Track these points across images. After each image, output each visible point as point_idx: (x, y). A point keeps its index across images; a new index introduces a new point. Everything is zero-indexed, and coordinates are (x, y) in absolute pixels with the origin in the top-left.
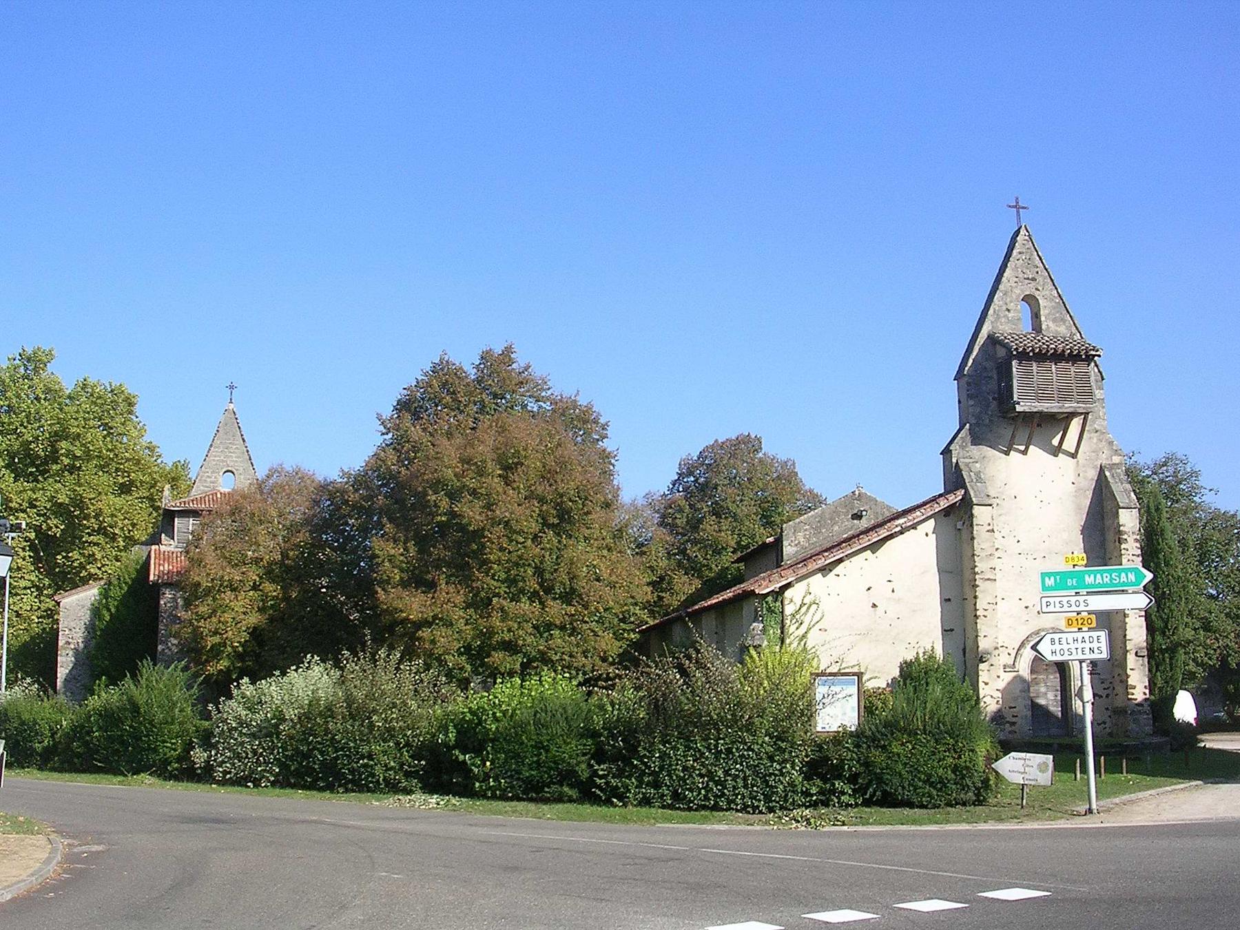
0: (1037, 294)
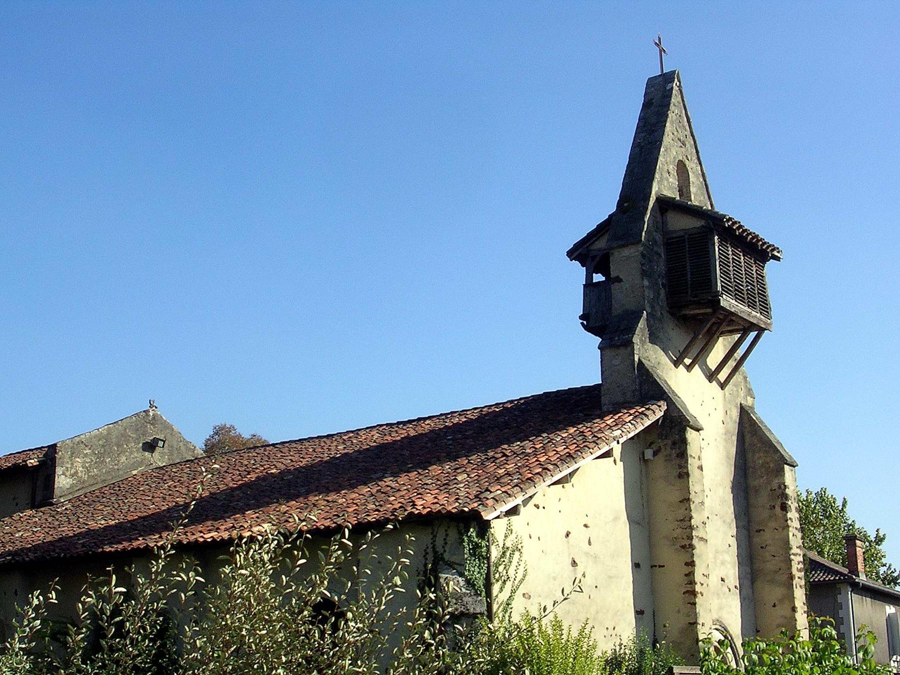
0: (687, 163)
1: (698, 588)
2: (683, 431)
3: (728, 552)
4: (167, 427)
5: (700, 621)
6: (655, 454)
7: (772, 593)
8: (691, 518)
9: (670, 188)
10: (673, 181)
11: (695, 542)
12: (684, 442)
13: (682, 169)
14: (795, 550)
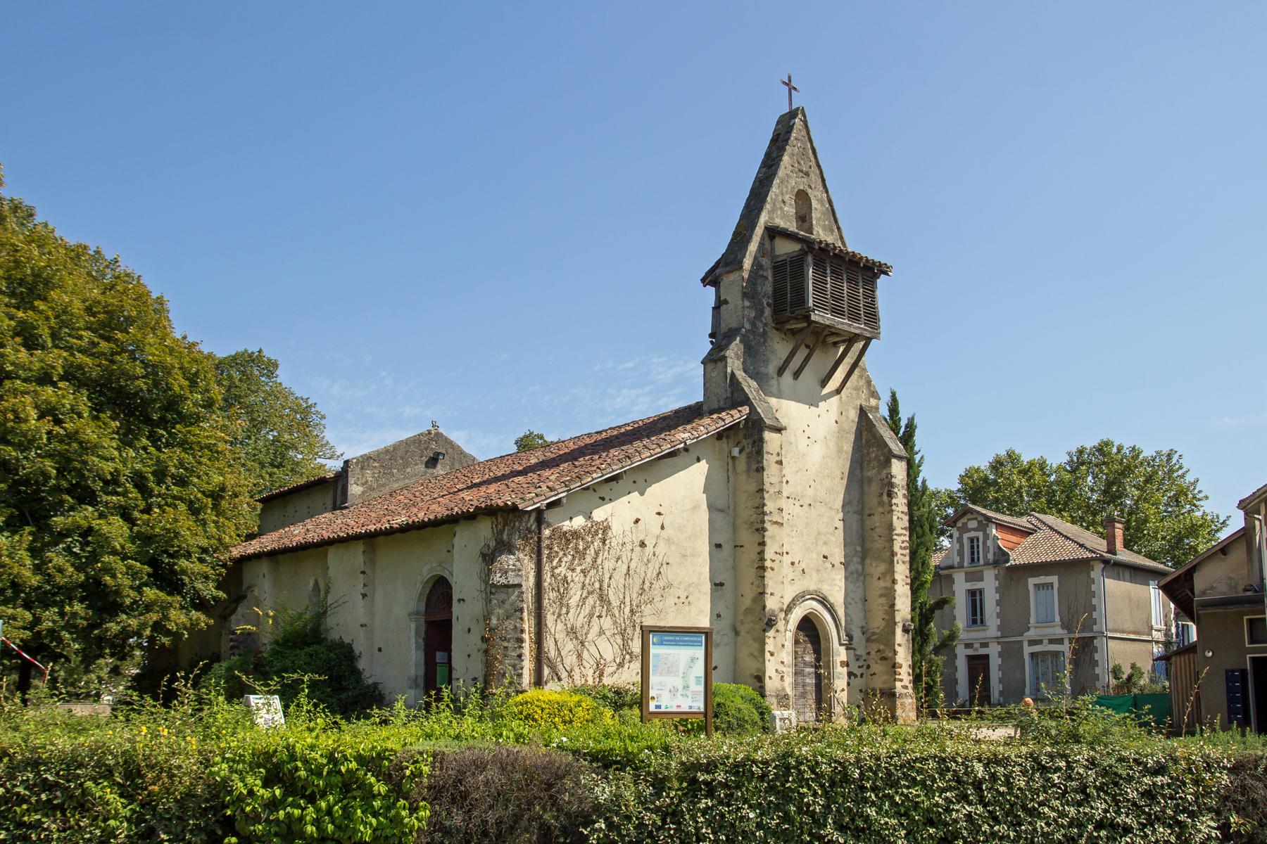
0: (809, 191)
1: (768, 564)
2: (761, 431)
3: (833, 534)
4: (448, 442)
5: (769, 591)
6: (741, 452)
7: (877, 569)
8: (764, 505)
9: (784, 216)
10: (790, 210)
11: (767, 525)
12: (761, 440)
13: (802, 198)
14: (898, 531)
